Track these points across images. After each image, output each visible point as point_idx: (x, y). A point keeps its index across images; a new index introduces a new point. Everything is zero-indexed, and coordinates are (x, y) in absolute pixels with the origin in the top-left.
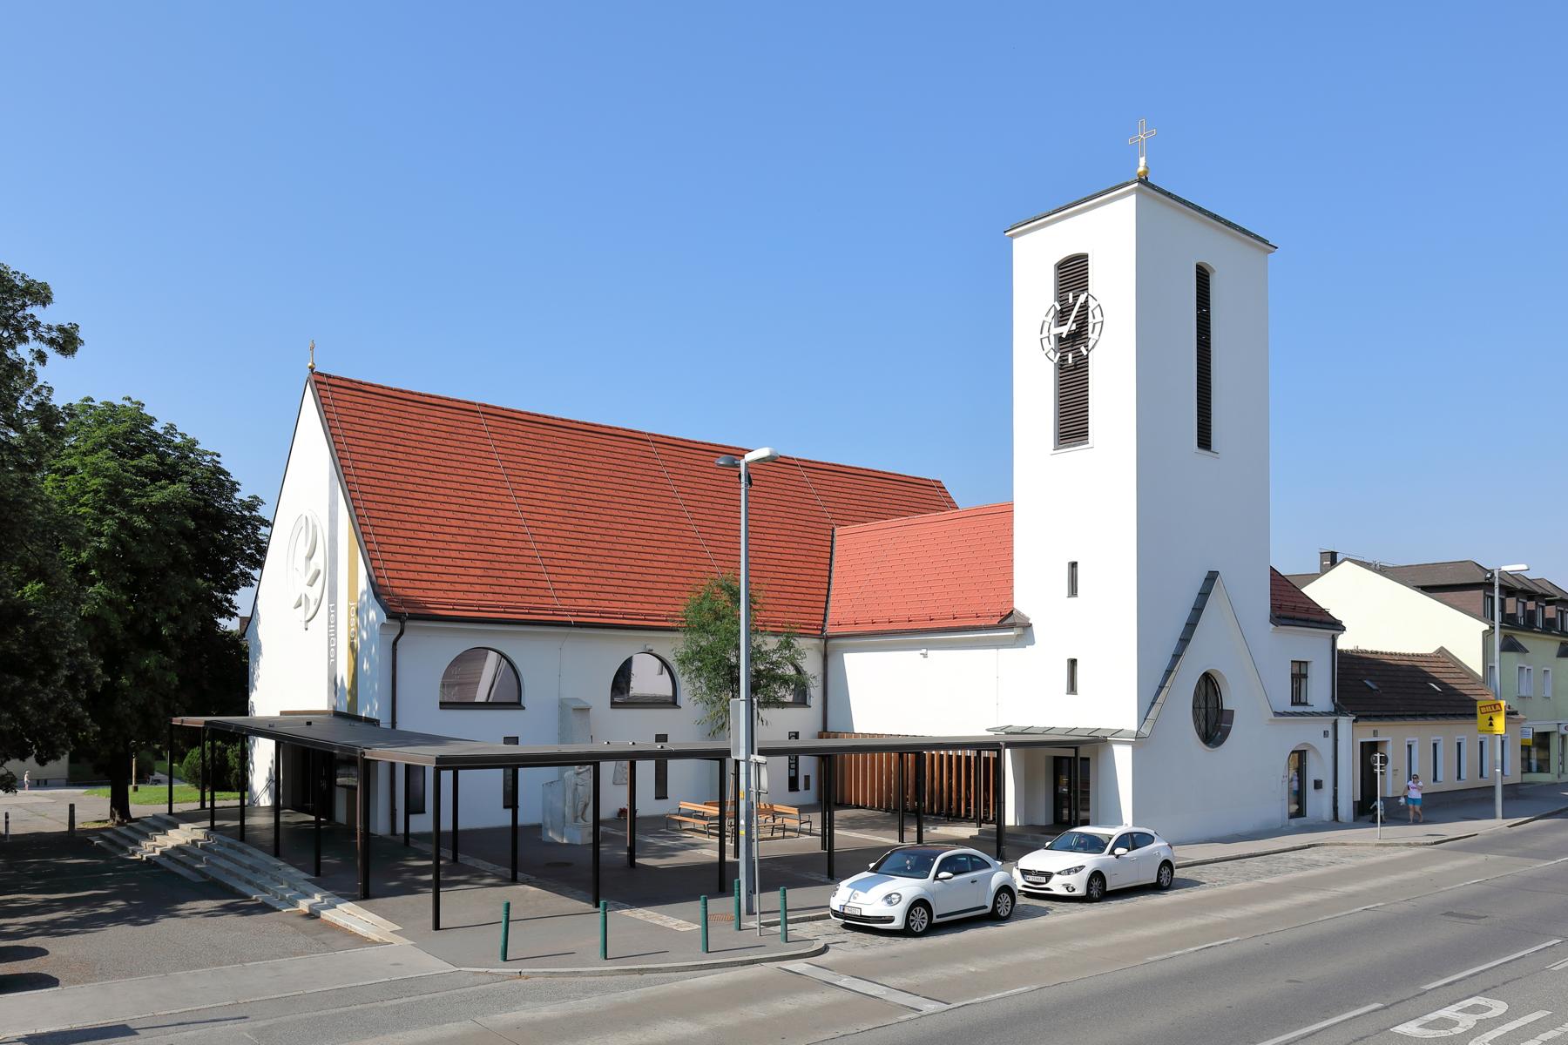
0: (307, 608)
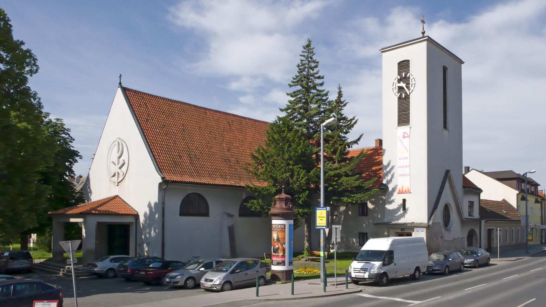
0: (118, 177)
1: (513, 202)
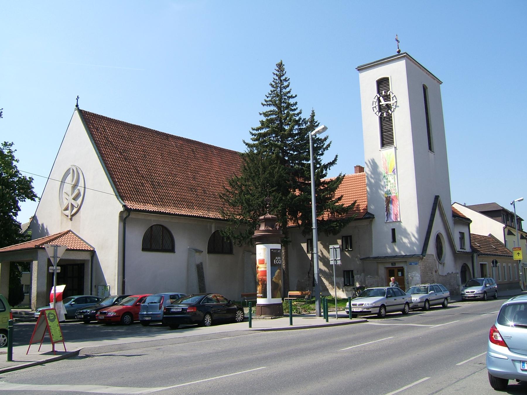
1: (500, 236)
